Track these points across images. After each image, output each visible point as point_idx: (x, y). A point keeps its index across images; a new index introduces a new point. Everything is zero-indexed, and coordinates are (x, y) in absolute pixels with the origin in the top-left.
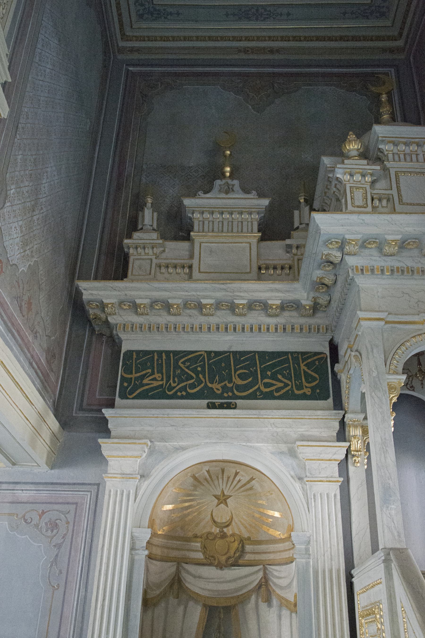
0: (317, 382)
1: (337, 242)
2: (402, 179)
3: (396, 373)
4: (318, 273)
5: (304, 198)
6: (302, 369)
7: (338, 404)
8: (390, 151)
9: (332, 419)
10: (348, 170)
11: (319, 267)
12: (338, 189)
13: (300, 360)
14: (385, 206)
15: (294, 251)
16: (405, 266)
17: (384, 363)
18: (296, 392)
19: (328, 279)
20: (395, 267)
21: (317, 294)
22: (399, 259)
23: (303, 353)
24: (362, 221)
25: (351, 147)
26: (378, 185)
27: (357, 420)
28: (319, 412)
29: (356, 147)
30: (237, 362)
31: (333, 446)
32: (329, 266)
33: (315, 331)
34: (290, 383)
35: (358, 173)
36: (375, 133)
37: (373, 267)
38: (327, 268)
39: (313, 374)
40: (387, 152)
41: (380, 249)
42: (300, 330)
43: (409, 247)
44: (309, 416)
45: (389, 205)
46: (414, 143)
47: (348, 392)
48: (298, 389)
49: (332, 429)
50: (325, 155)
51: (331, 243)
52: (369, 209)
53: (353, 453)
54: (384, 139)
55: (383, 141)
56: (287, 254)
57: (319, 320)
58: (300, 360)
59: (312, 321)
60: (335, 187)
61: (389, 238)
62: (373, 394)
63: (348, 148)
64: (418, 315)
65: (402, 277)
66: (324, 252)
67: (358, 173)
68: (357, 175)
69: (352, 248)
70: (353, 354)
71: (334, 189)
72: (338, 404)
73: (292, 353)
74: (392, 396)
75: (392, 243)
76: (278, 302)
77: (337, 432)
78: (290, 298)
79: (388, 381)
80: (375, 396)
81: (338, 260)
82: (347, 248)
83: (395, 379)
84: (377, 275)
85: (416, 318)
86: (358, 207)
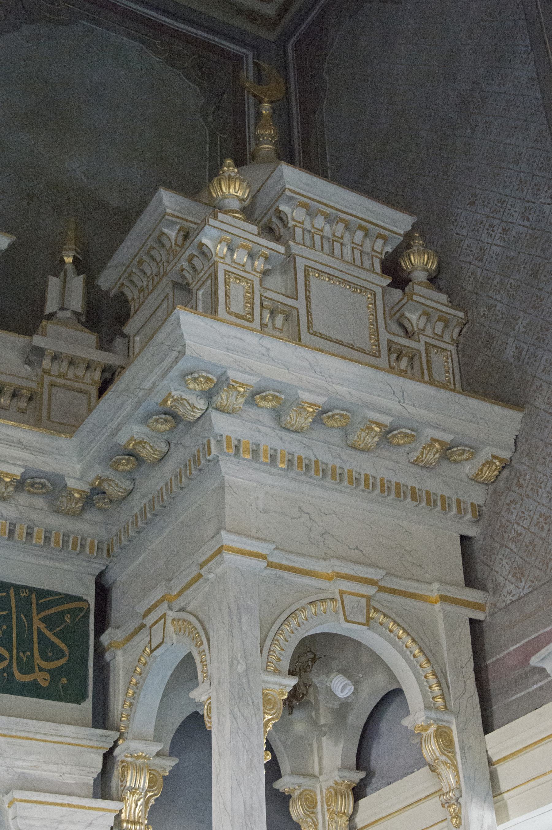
0: (64, 660)
1: (207, 379)
2: (314, 280)
3: (277, 672)
4: (137, 430)
5: (74, 257)
6: (35, 628)
7: (101, 718)
8: (300, 222)
9: (91, 747)
10: (228, 237)
11: (145, 419)
12: (194, 268)
13: (34, 606)
14: (280, 327)
15: (46, 363)
16: (313, 459)
17: (259, 649)
18: (19, 676)
19: (151, 447)
20: (296, 455)
21: (108, 473)
22: (307, 441)
23: (41, 593)
24: (264, 351)
25: (232, 191)
26: (270, 282)
27: (145, 756)
28: (69, 730)
29: (240, 194)
30: (24, 605)
31: (90, 808)
32: (166, 421)
33: (74, 547)
34: (6, 654)
35: (244, 247)
36: (281, 177)
37: (258, 445)
38: (159, 426)
39: (57, 641)
40: (294, 223)
41: (278, 415)
42: (45, 541)
43: (330, 423)
44: (46, 734)
45: (286, 326)
46: (342, 220)
47: (134, 693)
48: (21, 671)
49: (88, 769)
50: (170, 186)
51: (195, 380)
52: (256, 324)
53: (125, 825)
54: (295, 195)
55: (291, 199)
56: (27, 367)
57: (90, 527)
58: (34, 606)
59: (72, 525)
60: (190, 261)
61: (305, 396)
62: (236, 709)
63: (224, 190)
64: (325, 559)
65: (303, 478)
66: (173, 393)
67: (244, 247)
68: (241, 250)
69: (232, 400)
70: (171, 614)
71: (185, 264)
72: (101, 718)
73: (18, 588)
74: (268, 717)
75: (308, 409)
76: (18, 471)
77: (95, 776)
78: (46, 469)
79: (263, 685)
80: (239, 715)
81: (194, 416)
82: (224, 396)
83: (276, 683)
84: (262, 463)
85: (320, 566)
86: (236, 315)
